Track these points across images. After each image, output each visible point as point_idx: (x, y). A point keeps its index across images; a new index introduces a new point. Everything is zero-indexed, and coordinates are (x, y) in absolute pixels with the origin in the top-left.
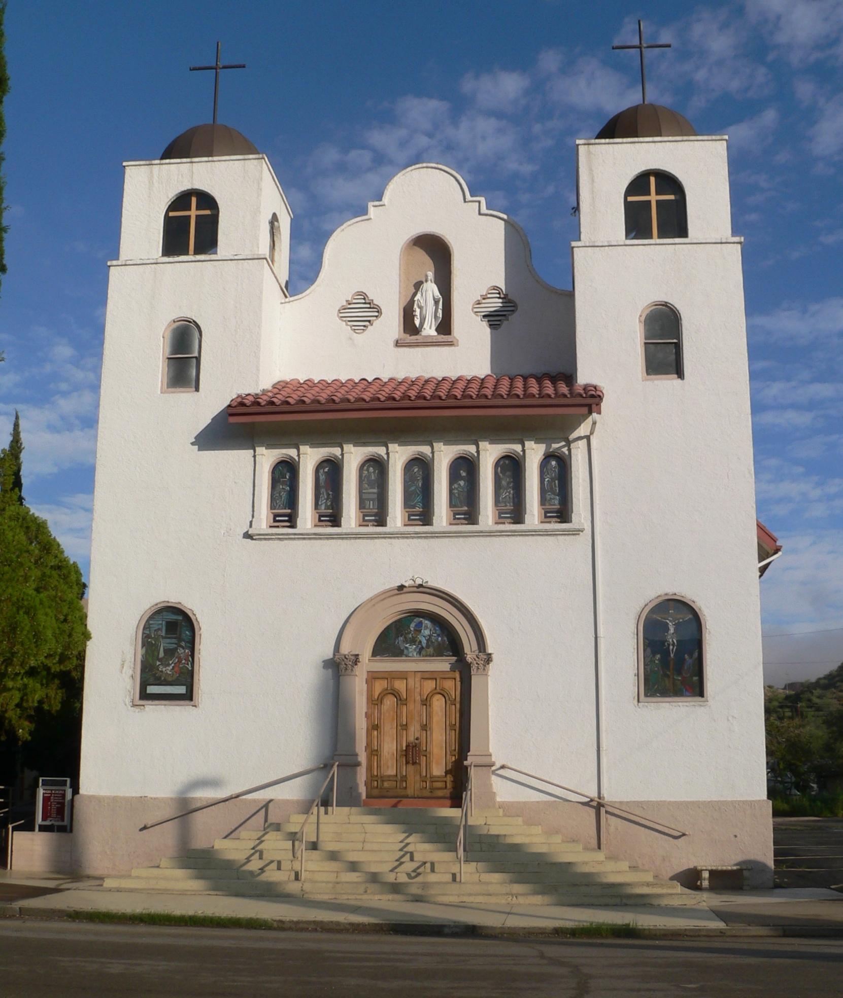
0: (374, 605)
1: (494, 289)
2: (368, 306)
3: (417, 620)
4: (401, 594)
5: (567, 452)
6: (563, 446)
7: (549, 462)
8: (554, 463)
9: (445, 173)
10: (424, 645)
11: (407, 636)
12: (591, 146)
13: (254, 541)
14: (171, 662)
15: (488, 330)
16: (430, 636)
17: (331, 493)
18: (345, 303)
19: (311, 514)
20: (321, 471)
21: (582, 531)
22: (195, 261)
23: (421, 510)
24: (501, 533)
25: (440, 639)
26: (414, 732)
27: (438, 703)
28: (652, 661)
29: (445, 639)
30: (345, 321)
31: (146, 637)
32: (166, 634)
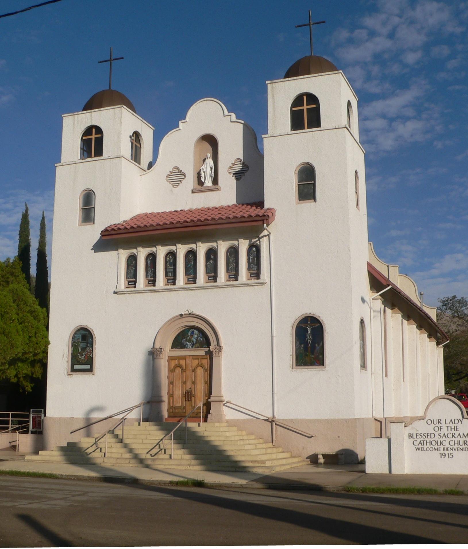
0: (170, 324)
1: (238, 160)
2: (180, 173)
3: (191, 330)
4: (182, 318)
5: (259, 244)
6: (257, 241)
7: (252, 248)
8: (254, 249)
9: (215, 103)
10: (195, 343)
11: (187, 338)
12: (273, 84)
13: (118, 295)
14: (84, 354)
15: (235, 181)
16: (197, 338)
17: (153, 270)
18: (169, 173)
19: (143, 281)
20: (149, 259)
21: (265, 283)
22: (92, 161)
23: (193, 276)
24: (227, 286)
25: (202, 339)
26: (189, 385)
27: (200, 370)
28: (300, 348)
29: (204, 339)
30: (169, 182)
31: (73, 342)
32: (82, 340)
